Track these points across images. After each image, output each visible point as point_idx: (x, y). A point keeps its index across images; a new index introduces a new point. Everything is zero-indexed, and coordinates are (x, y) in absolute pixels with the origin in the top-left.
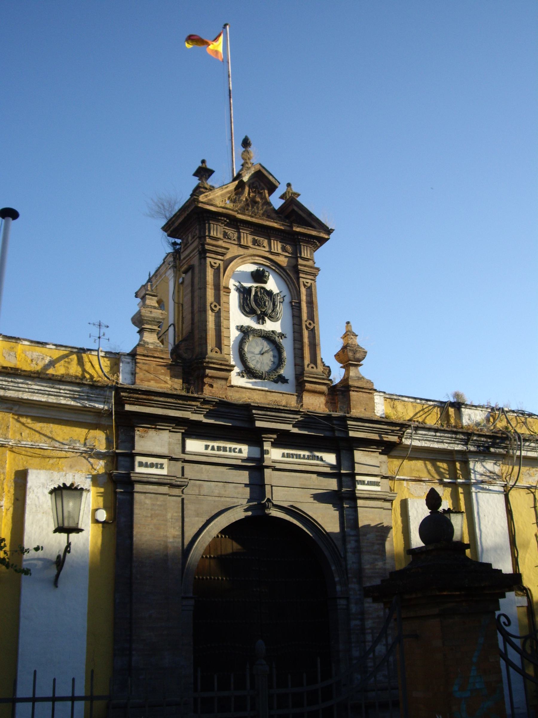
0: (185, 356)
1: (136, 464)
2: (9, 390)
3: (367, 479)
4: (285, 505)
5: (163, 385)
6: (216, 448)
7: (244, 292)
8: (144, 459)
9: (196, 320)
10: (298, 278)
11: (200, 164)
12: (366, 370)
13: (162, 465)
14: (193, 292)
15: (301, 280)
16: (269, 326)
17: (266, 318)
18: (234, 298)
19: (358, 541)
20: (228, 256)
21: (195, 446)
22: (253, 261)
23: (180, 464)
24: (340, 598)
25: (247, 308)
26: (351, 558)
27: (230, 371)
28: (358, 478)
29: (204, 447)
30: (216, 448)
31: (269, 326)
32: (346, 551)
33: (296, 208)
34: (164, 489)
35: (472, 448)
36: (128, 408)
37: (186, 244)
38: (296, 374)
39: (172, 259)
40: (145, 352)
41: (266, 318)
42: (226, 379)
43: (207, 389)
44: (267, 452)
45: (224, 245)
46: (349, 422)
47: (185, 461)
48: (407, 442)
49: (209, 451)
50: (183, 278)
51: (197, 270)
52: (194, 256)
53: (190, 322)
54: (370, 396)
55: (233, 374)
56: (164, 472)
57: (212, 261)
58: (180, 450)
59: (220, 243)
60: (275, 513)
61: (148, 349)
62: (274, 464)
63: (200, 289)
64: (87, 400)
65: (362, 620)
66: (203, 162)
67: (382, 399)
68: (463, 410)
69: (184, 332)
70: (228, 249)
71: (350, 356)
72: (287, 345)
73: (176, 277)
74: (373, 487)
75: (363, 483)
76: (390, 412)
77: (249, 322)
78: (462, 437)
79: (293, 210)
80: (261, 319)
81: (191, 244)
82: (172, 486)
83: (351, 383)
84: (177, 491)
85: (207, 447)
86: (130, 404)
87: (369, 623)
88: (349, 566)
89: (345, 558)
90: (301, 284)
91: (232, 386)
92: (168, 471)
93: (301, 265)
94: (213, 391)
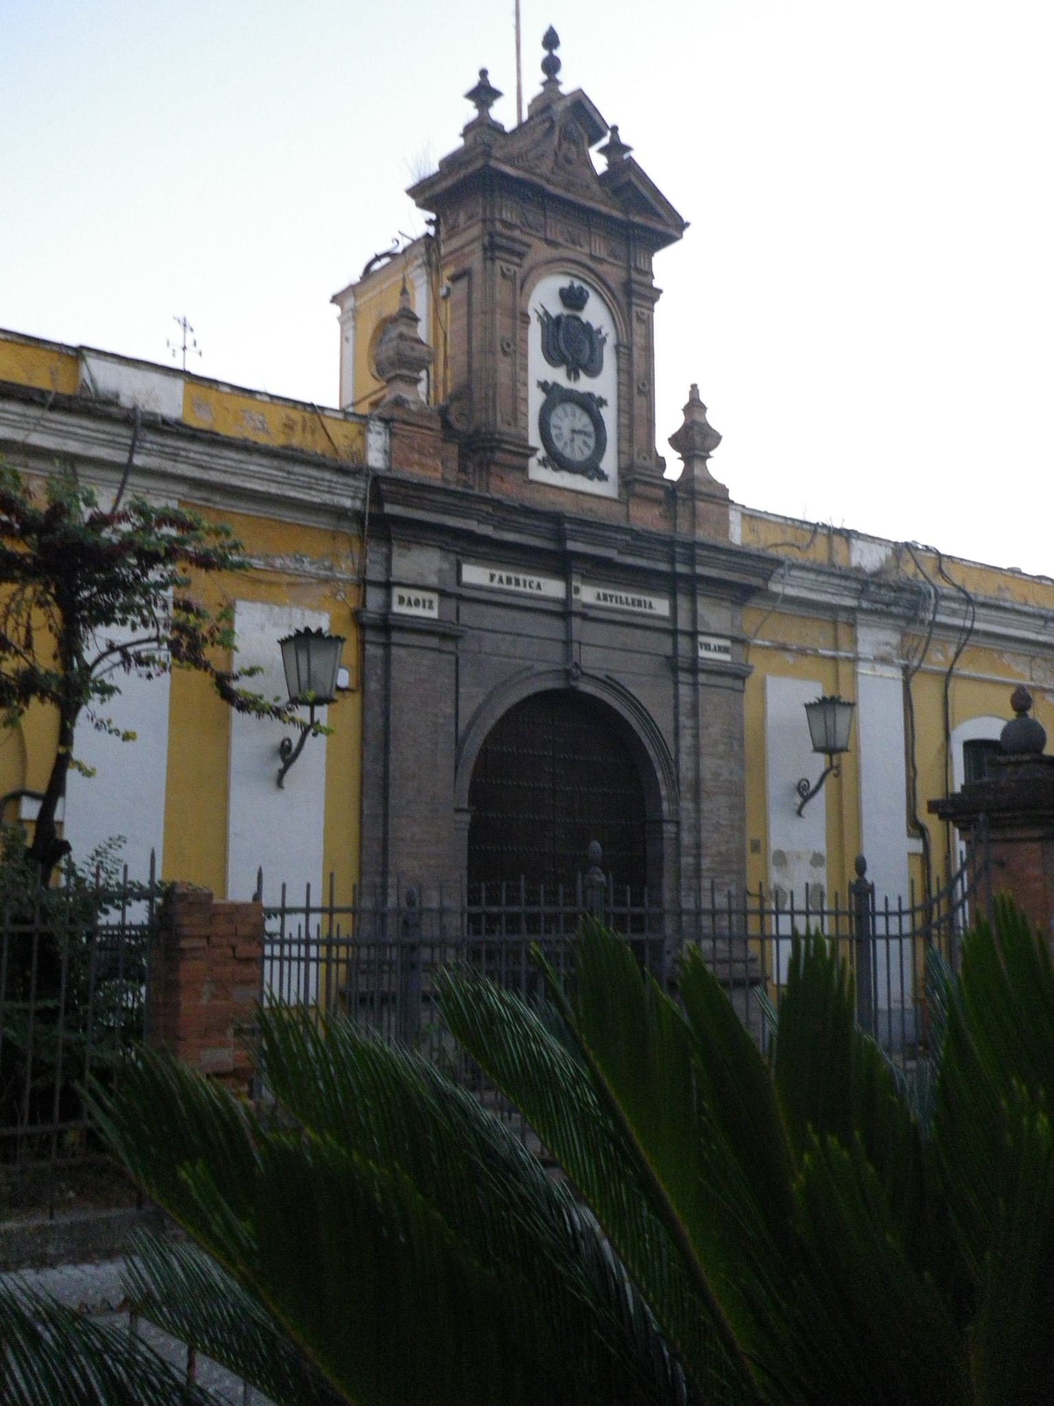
0: (458, 426)
1: (395, 599)
2: (211, 469)
3: (714, 642)
4: (601, 675)
5: (430, 473)
6: (504, 580)
7: (552, 325)
8: (406, 593)
9: (475, 365)
10: (630, 304)
11: (470, 112)
12: (718, 466)
13: (431, 602)
14: (470, 315)
15: (634, 308)
16: (584, 384)
17: (581, 373)
18: (535, 334)
19: (696, 737)
20: (528, 262)
21: (474, 574)
22: (561, 269)
23: (452, 604)
24: (668, 822)
25: (553, 355)
26: (686, 762)
27: (528, 456)
28: (701, 639)
29: (488, 577)
30: (504, 580)
31: (584, 384)
32: (677, 752)
33: (634, 179)
34: (433, 642)
35: (865, 605)
36: (389, 509)
37: (453, 227)
38: (620, 468)
39: (423, 250)
40: (406, 417)
41: (581, 373)
42: (524, 469)
43: (494, 481)
44: (577, 590)
45: (525, 238)
46: (699, 551)
47: (460, 598)
48: (775, 587)
49: (496, 584)
50: (448, 289)
51: (478, 279)
52: (473, 252)
53: (466, 368)
54: (723, 509)
55: (533, 462)
56: (434, 614)
57: (505, 266)
58: (454, 580)
59: (517, 234)
60: (586, 687)
61: (409, 411)
62: (585, 610)
63: (485, 313)
64: (328, 492)
65: (698, 856)
66: (483, 73)
67: (739, 515)
68: (853, 541)
69: (449, 384)
70: (529, 246)
71: (696, 438)
72: (609, 415)
73: (433, 286)
74: (46, 437)
75: (707, 647)
76: (751, 538)
77: (558, 375)
78: (854, 585)
79: (630, 183)
80: (573, 373)
81: (464, 230)
82: (444, 636)
83: (697, 487)
84: (449, 646)
85: (492, 577)
86: (392, 503)
87: (706, 863)
88: (681, 775)
89: (677, 762)
90: (634, 315)
91: (531, 482)
92: (440, 613)
93: (636, 282)
94: (503, 488)
